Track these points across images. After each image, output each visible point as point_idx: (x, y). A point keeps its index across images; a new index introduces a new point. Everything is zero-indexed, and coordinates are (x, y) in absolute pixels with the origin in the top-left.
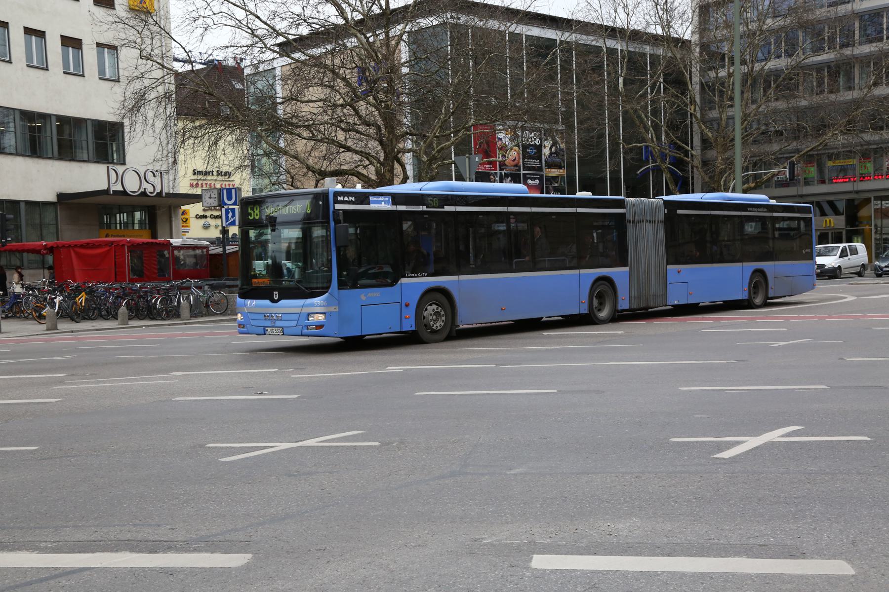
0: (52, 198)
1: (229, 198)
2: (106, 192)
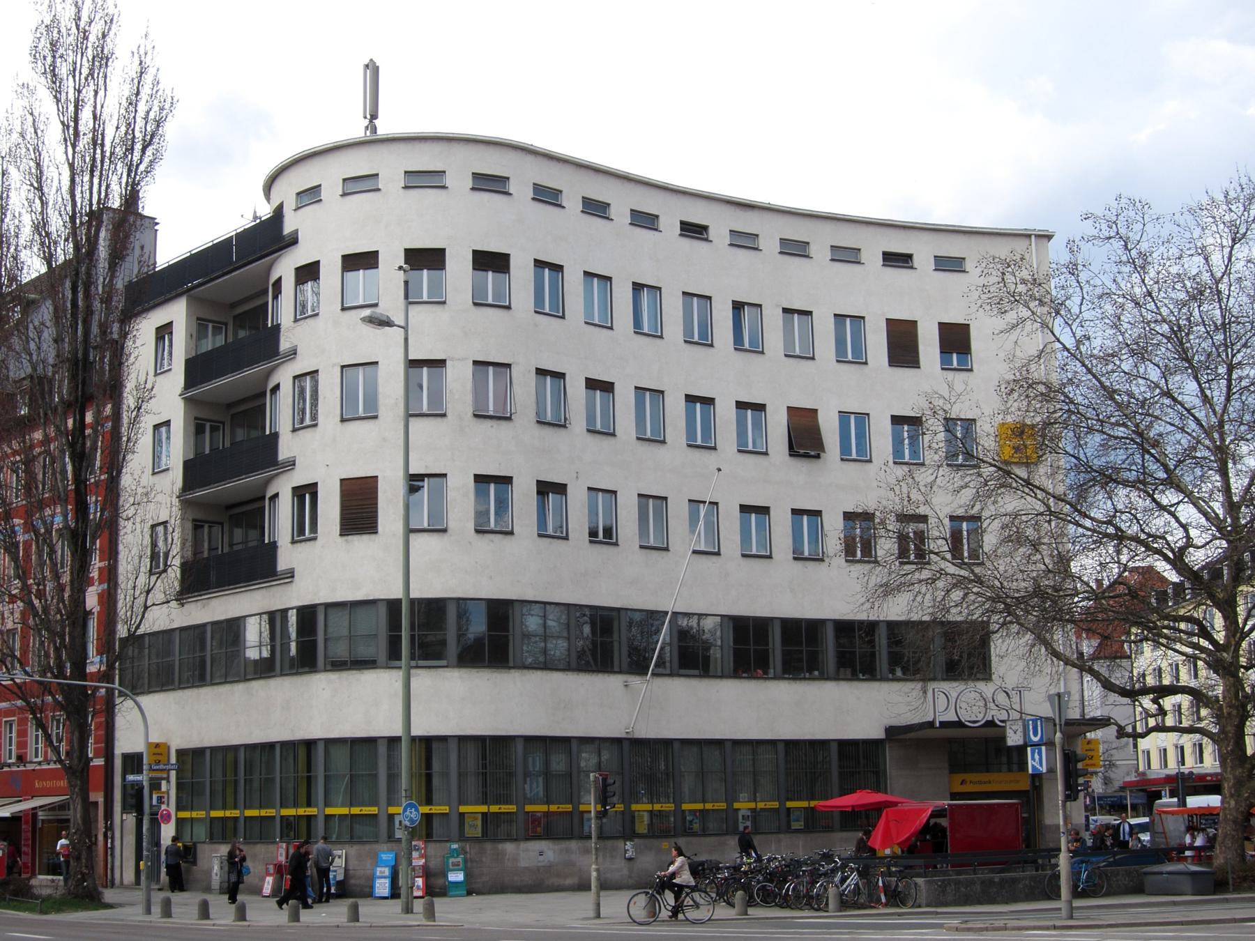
0: (877, 733)
1: (1035, 735)
2: (931, 724)
